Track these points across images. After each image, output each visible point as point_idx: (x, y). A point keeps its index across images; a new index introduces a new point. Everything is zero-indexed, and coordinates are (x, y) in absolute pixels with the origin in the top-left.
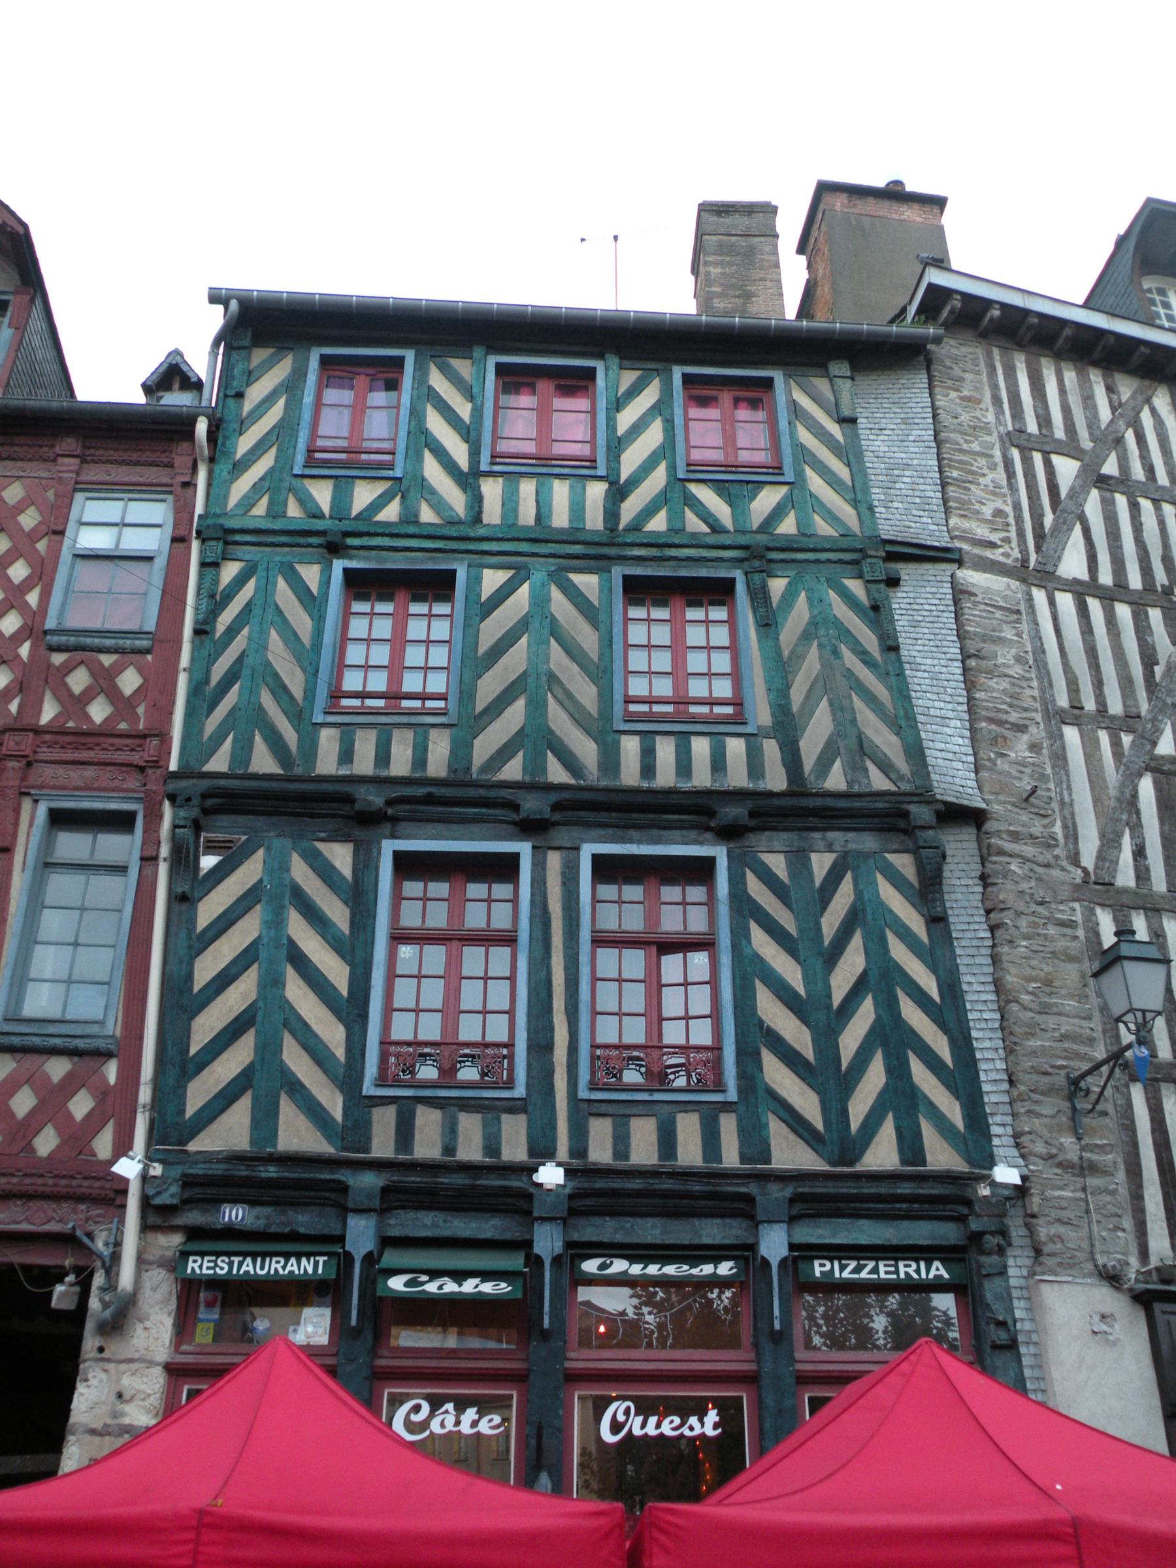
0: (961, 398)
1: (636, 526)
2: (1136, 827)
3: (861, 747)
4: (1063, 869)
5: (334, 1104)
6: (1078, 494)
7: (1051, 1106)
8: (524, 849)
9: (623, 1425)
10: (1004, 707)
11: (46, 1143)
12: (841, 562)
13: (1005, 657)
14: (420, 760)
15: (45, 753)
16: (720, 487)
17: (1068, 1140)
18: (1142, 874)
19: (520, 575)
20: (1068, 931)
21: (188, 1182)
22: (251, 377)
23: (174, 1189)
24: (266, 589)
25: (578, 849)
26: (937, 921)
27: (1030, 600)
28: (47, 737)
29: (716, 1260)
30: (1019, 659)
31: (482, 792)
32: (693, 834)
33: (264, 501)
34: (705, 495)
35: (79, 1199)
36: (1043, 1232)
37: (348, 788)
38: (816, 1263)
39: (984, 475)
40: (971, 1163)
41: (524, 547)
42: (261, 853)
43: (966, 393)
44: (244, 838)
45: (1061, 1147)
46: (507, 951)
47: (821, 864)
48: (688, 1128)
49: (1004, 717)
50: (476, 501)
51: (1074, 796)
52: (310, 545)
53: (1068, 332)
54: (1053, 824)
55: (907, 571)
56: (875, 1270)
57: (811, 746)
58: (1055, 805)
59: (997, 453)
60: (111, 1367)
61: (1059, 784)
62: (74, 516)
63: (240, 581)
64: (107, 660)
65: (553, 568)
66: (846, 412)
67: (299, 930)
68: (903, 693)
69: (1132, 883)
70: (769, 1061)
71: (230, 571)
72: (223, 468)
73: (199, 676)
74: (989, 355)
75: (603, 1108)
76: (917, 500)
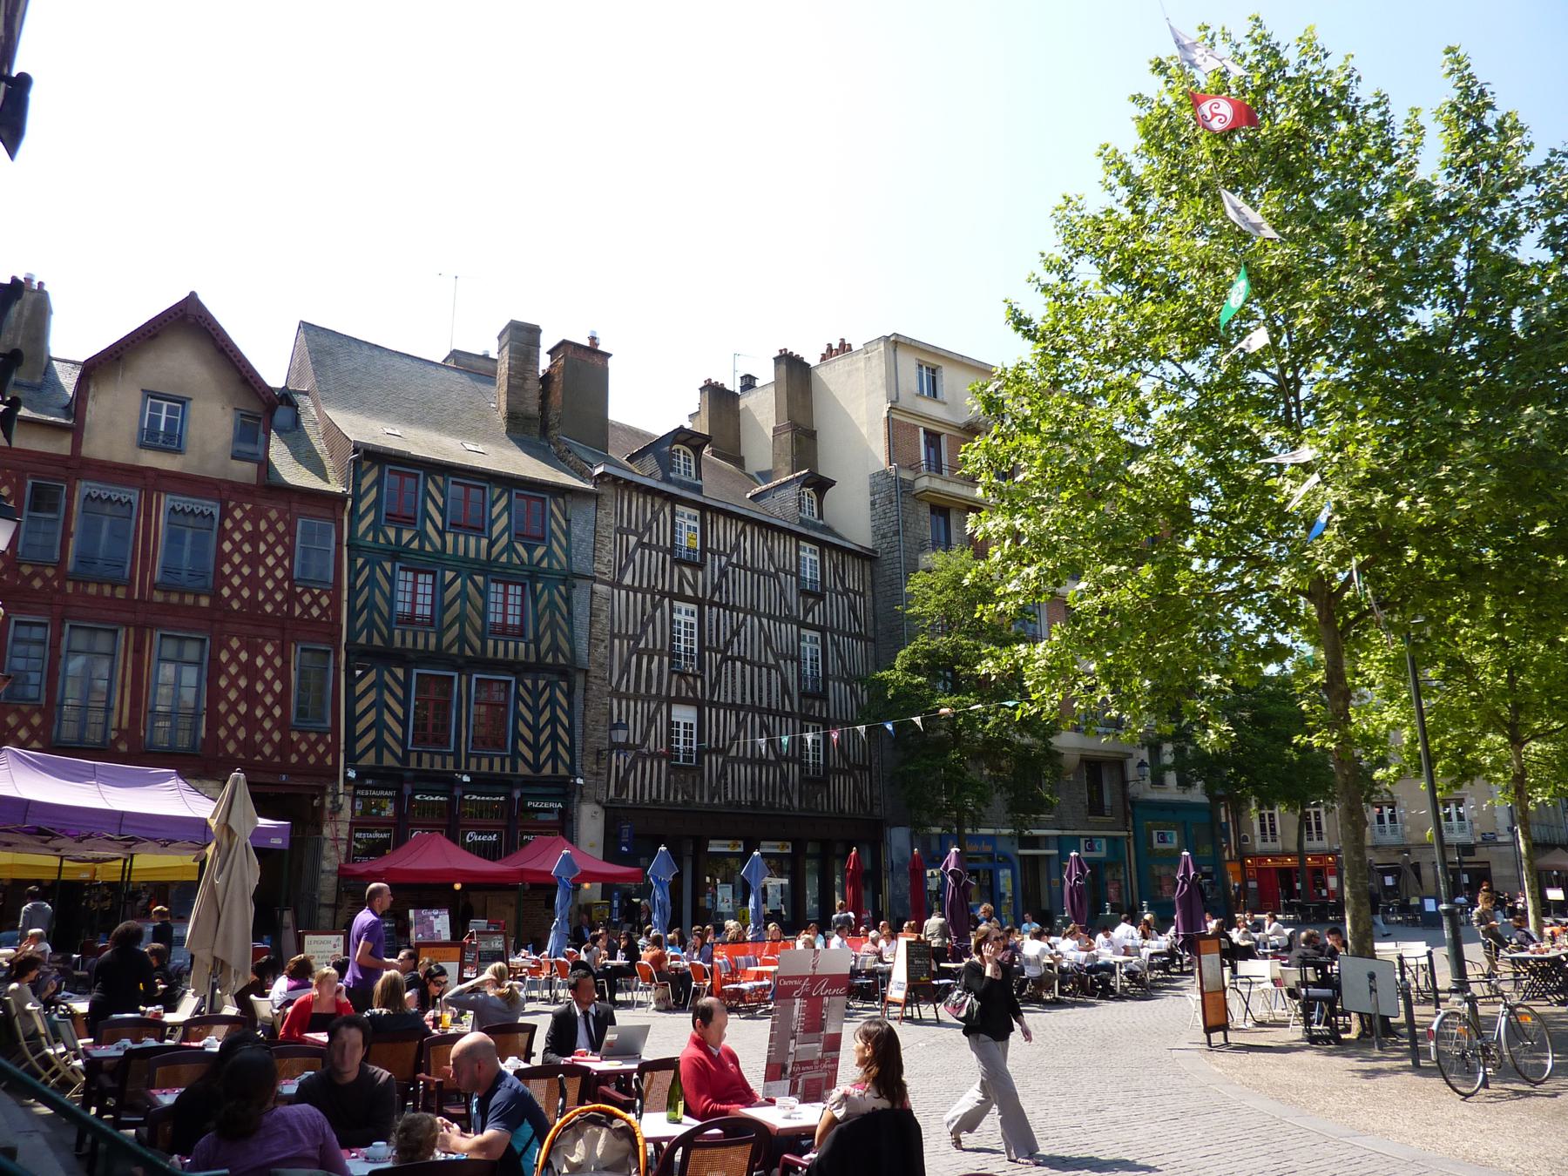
5: (400, 752)
7: (592, 758)
11: (312, 759)
18: (628, 688)
24: (372, 571)
26: (571, 704)
34: (520, 548)
48: (497, 762)
55: (578, 582)
57: (544, 646)
63: (363, 567)
68: (571, 629)
70: (520, 743)
71: (360, 561)
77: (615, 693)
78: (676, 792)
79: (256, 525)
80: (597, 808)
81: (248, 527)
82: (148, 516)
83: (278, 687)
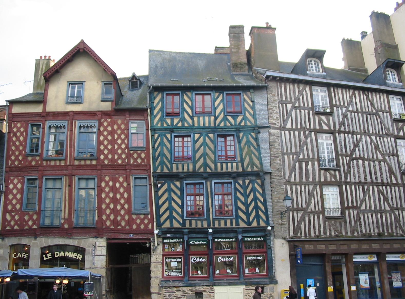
0: (272, 95)
1: (219, 125)
2: (295, 172)
3: (253, 164)
4: (283, 180)
5: (181, 220)
6: (291, 111)
8: (204, 182)
9: (221, 260)
10: (275, 154)
11: (142, 227)
12: (251, 130)
13: (276, 145)
14: (188, 169)
15: (133, 168)
16: (233, 117)
17: (280, 221)
19: (201, 135)
20: (282, 190)
21: (162, 232)
22: (155, 98)
23: (161, 233)
24: (162, 139)
25: (212, 181)
26: (264, 190)
27: (281, 133)
28: (132, 166)
29: (232, 239)
30: (279, 145)
31: (197, 174)
32: (228, 178)
33: (160, 123)
34: (230, 118)
35: (148, 234)
36: (275, 234)
37: (178, 174)
38: (246, 239)
39: (275, 110)
40: (266, 225)
41: (201, 130)
42: (166, 183)
43: (273, 94)
44: (164, 181)
45: (279, 222)
46: (202, 196)
47: (247, 182)
48: (228, 222)
49: (275, 156)
50: (193, 121)
51: (286, 168)
52: (168, 131)
53: (290, 80)
54: (282, 173)
55: (261, 130)
56: (253, 239)
57: (246, 164)
58: (282, 170)
59: (277, 106)
60: (155, 255)
61: (283, 166)
62: (130, 126)
63: (158, 138)
64: (139, 152)
65: (206, 133)
66: (253, 100)
67: (173, 195)
68: (260, 154)
69: (293, 181)
70: (239, 212)
71: (156, 136)
72: (153, 117)
73: (154, 155)
74: (277, 85)
75: (217, 219)
76: (264, 117)
77: (288, 182)
78: (330, 230)
79: (113, 128)
80: (283, 241)
81: (109, 128)
82: (71, 130)
83: (126, 195)
